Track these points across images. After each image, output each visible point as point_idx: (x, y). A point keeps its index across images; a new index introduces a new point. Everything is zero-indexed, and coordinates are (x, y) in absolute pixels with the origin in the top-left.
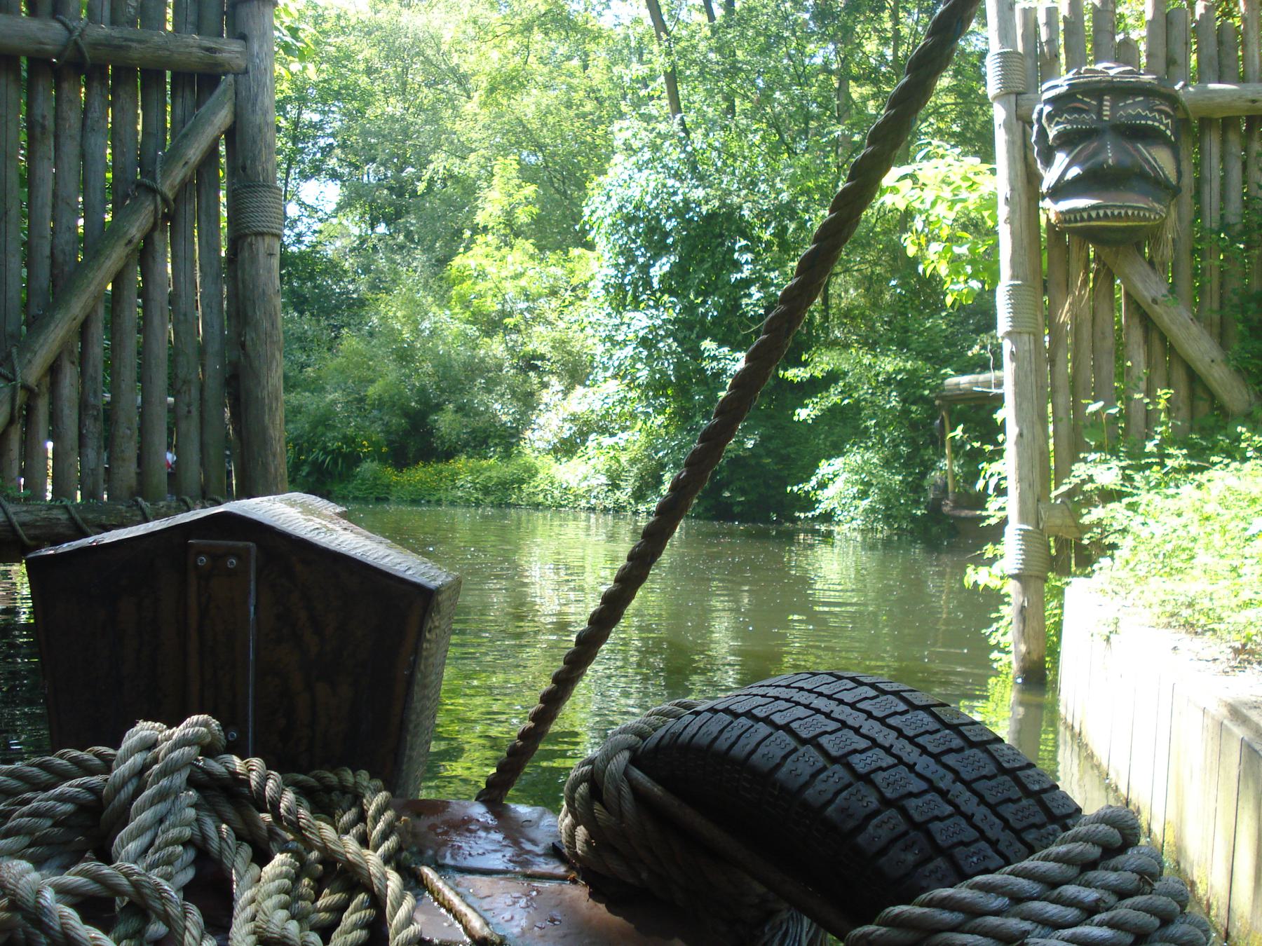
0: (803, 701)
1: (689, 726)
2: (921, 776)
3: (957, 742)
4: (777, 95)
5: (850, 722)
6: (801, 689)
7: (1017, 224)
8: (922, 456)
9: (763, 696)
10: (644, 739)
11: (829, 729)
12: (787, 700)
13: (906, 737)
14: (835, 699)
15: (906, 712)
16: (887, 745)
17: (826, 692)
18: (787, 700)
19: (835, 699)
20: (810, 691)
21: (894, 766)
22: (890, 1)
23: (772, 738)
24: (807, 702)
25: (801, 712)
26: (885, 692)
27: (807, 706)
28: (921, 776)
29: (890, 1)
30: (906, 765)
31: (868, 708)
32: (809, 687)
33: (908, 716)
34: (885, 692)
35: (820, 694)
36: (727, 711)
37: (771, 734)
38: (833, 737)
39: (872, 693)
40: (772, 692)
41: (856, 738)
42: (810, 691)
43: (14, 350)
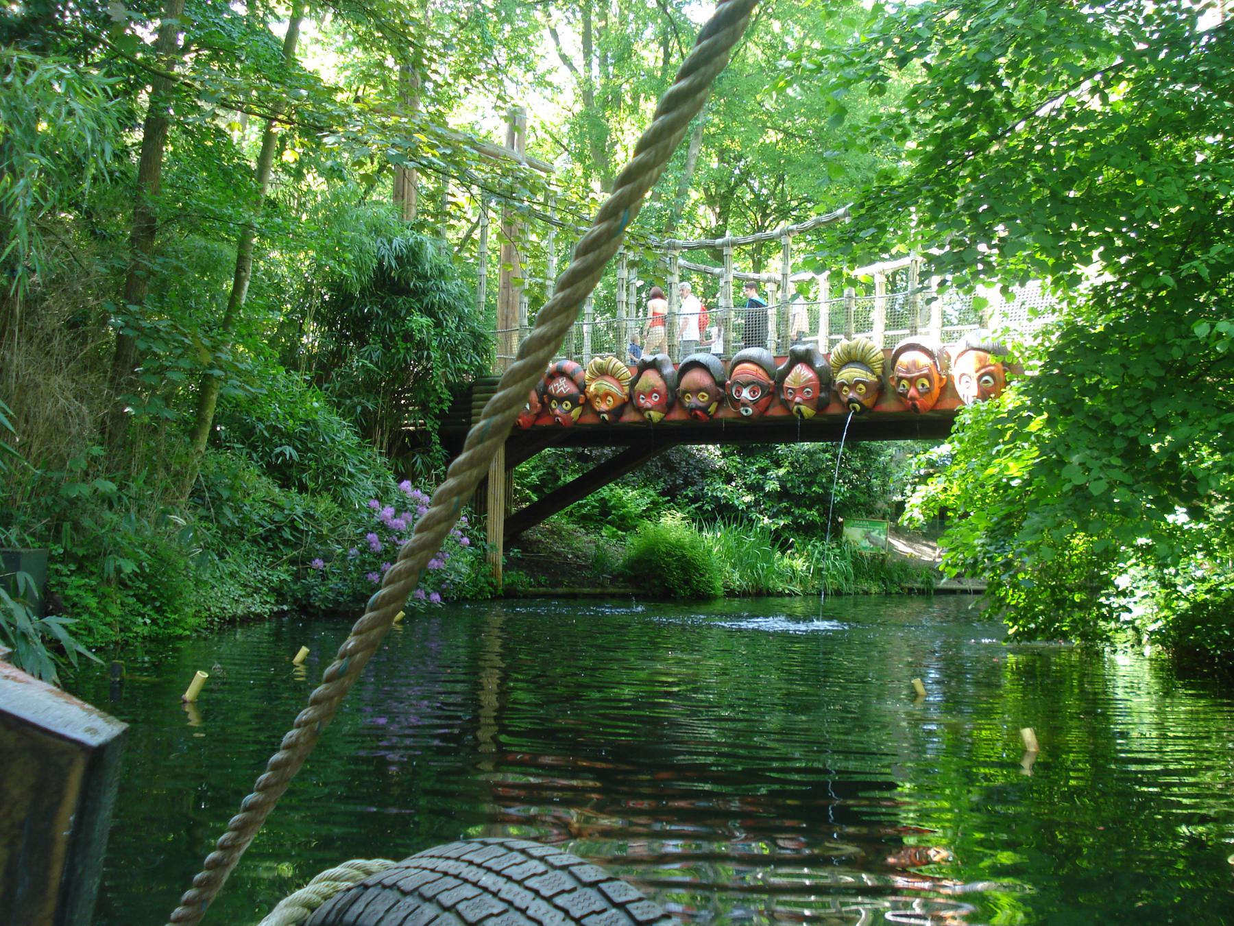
0: (471, 877)
2: (502, 900)
3: (569, 884)
5: (518, 902)
6: (471, 863)
7: (930, 414)
10: (312, 909)
11: (495, 911)
12: (456, 877)
13: (543, 898)
14: (504, 876)
16: (524, 907)
18: (456, 877)
20: (479, 866)
21: (505, 911)
23: (438, 921)
25: (468, 891)
27: (475, 884)
28: (502, 900)
30: (518, 909)
31: (567, 905)
33: (575, 894)
34: (554, 867)
35: (489, 870)
36: (393, 886)
37: (437, 917)
38: (498, 920)
39: (541, 868)
40: (442, 865)
41: (495, 901)
43: (1033, 200)
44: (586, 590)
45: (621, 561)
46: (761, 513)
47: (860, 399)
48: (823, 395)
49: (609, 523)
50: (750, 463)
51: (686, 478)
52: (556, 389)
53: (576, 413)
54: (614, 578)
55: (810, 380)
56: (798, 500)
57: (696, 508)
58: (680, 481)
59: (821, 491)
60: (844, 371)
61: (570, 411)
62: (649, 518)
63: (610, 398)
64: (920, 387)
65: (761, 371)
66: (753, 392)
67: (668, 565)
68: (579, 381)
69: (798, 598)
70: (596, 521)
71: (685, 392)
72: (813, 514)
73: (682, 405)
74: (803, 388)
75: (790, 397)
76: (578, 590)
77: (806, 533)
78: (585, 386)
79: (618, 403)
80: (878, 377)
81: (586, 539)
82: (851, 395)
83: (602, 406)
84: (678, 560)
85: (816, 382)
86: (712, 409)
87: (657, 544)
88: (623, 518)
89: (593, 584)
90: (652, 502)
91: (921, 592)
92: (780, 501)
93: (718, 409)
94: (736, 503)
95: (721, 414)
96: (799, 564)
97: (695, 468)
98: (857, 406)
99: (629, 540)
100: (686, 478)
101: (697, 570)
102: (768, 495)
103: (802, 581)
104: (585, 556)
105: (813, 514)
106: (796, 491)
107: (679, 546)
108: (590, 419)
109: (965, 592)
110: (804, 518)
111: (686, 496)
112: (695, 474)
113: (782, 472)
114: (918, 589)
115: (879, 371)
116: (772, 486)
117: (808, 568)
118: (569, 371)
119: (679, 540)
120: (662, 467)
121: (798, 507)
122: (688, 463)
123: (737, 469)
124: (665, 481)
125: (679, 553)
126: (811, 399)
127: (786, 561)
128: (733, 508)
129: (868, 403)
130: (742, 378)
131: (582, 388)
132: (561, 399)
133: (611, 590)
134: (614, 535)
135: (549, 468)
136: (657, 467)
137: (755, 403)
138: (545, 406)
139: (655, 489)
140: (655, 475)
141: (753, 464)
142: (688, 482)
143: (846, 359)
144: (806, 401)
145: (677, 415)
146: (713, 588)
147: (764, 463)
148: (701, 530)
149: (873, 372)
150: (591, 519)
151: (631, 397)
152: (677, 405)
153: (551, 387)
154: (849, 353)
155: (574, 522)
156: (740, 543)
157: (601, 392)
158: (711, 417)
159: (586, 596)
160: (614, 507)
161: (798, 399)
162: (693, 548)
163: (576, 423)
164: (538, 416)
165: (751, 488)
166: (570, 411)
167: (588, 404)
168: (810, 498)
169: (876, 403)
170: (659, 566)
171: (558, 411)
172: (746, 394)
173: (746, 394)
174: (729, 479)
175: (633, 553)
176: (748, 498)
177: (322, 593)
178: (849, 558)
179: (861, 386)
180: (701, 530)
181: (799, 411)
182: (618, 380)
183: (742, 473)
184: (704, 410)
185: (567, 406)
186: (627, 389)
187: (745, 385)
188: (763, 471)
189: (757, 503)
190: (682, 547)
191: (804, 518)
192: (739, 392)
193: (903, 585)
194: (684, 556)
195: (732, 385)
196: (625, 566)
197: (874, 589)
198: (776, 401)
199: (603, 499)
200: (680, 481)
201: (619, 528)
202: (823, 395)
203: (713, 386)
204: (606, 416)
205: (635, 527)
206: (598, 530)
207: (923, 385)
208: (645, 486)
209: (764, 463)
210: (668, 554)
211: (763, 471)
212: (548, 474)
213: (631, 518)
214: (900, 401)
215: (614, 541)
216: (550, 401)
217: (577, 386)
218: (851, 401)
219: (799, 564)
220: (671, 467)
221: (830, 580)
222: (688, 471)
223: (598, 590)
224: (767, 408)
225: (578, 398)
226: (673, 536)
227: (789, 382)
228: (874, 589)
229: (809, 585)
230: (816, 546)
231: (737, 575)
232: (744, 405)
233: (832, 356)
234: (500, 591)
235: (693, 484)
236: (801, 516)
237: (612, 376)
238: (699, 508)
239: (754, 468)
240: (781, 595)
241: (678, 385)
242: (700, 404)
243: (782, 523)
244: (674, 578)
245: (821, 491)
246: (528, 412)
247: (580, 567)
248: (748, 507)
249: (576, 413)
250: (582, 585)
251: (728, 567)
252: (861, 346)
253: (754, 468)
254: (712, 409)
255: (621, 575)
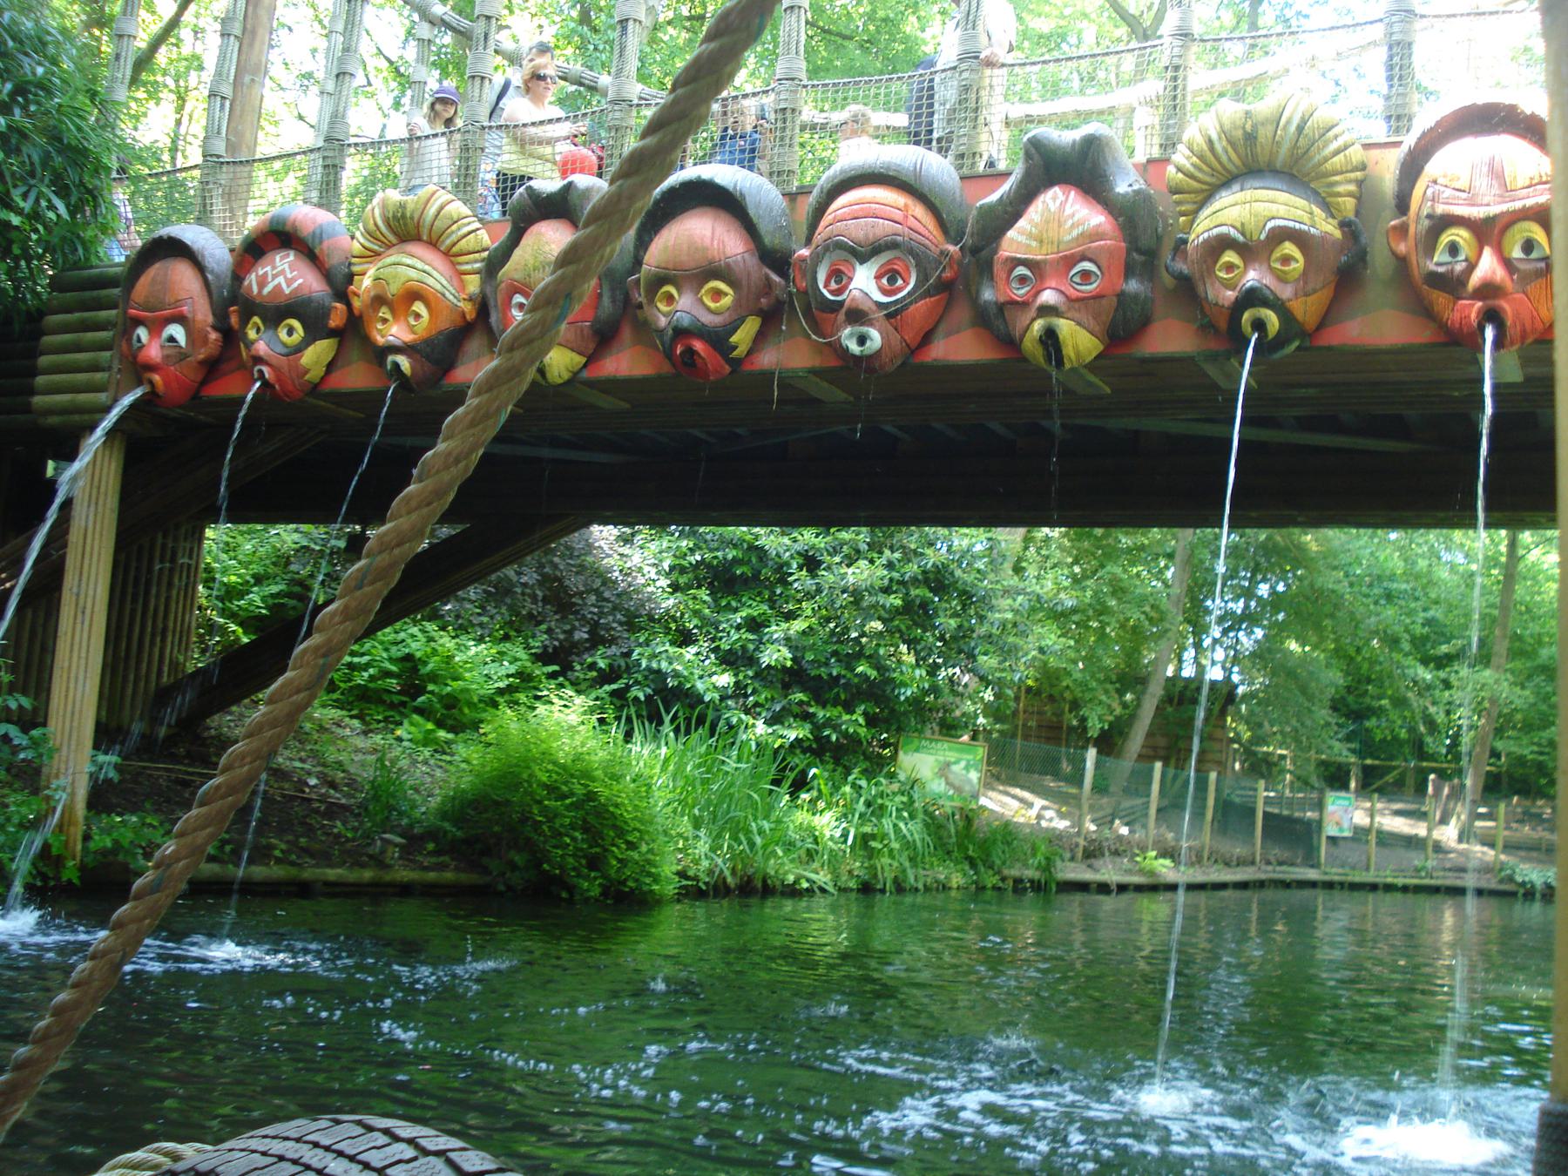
1: (247, 237)
4: (338, 1013)
6: (316, 1145)
8: (416, 1042)
9: (264, 1154)
14: (359, 1162)
15: (415, 1159)
17: (326, 1142)
19: (359, 1162)
20: (327, 1149)
22: (3, 992)
24: (296, 1156)
26: (426, 1152)
29: (3, 992)
32: (352, 1152)
34: (426, 1152)
35: (340, 1154)
39: (410, 1152)
42: (327, 1149)
44: (332, 874)
45: (434, 802)
46: (747, 712)
47: (1286, 292)
48: (1133, 286)
49: (420, 711)
50: (730, 609)
51: (594, 627)
52: (262, 283)
53: (317, 354)
54: (414, 841)
55: (1095, 235)
56: (820, 690)
57: (613, 694)
58: (581, 635)
59: (873, 674)
60: (1224, 199)
61: (299, 349)
62: (514, 704)
63: (419, 307)
64: (1517, 253)
65: (919, 210)
66: (890, 275)
67: (552, 816)
68: (334, 260)
69: (820, 900)
70: (392, 706)
71: (659, 281)
72: (854, 722)
73: (644, 329)
74: (1070, 261)
75: (1020, 293)
76: (312, 872)
77: (837, 761)
78: (350, 278)
79: (445, 323)
80: (1344, 225)
81: (360, 742)
82: (1253, 277)
83: (392, 331)
84: (576, 806)
85: (1113, 242)
86: (742, 337)
87: (526, 762)
88: (451, 702)
89: (355, 857)
90: (519, 674)
91: (1037, 887)
92: (786, 687)
93: (760, 338)
94: (700, 686)
95: (768, 359)
96: (827, 824)
97: (615, 608)
98: (1272, 319)
99: (462, 751)
100: (594, 627)
101: (621, 832)
102: (765, 675)
103: (834, 861)
104: (352, 783)
105: (854, 722)
106: (823, 671)
107: (578, 770)
108: (356, 377)
109: (1103, 888)
110: (836, 728)
111: (592, 666)
112: (613, 621)
113: (798, 625)
114: (1032, 881)
115: (1349, 204)
116: (774, 655)
117: (845, 835)
118: (306, 231)
119: (578, 758)
120: (545, 600)
121: (823, 704)
122: (601, 598)
123: (703, 618)
124: (549, 631)
125: (579, 790)
126: (1098, 297)
127: (801, 817)
128: (694, 699)
129: (1306, 310)
130: (859, 231)
131: (340, 285)
132: (276, 313)
133: (405, 874)
134: (428, 740)
135: (293, 582)
136: (534, 598)
137: (893, 314)
138: (231, 337)
139: (528, 647)
140: (531, 616)
141: (736, 610)
142: (596, 641)
143: (1231, 159)
144: (1076, 303)
145: (625, 363)
146: (656, 879)
147: (758, 609)
148: (628, 736)
149: (1327, 207)
150: (382, 702)
151: (483, 306)
152: (627, 333)
153: (252, 280)
154: (1250, 138)
155: (339, 705)
156: (711, 766)
157: (394, 289)
158: (736, 363)
159: (337, 890)
160: (433, 677)
161: (1048, 297)
162: (616, 778)
163: (315, 389)
164: (211, 368)
165: (729, 660)
166: (299, 349)
167: (353, 332)
168: (847, 686)
169: (1324, 321)
170: (525, 819)
171: (262, 348)
172: (864, 282)
173: (864, 282)
174: (685, 638)
175: (466, 783)
176: (725, 679)
177: (1539, 679)
178: (921, 816)
179: (1289, 248)
180: (628, 736)
181: (1050, 336)
182: (449, 255)
183: (711, 627)
184: (719, 339)
185: (292, 332)
186: (473, 284)
187: (862, 254)
188: (755, 625)
189: (739, 691)
190: (587, 775)
191: (836, 728)
192: (839, 276)
193: (1006, 872)
194: (591, 796)
195: (817, 259)
196: (443, 814)
197: (957, 880)
198: (961, 313)
199: (409, 658)
200: (581, 635)
201: (440, 724)
202: (1133, 286)
203: (752, 261)
204: (404, 363)
205: (475, 725)
206: (391, 723)
207: (1529, 246)
208: (506, 638)
209: (758, 609)
210: (551, 789)
211: (755, 625)
212: (289, 595)
213: (471, 705)
214: (1426, 312)
215: (427, 752)
216: (245, 320)
217: (326, 274)
218: (1252, 298)
219: (827, 824)
220: (560, 600)
221: (886, 860)
222: (601, 614)
223: (367, 875)
224: (927, 338)
225: (325, 313)
226: (564, 749)
227: (1018, 240)
228: (957, 880)
229: (844, 869)
230: (857, 786)
231: (703, 847)
232: (857, 316)
233: (1181, 156)
234: (70, 873)
235: (612, 641)
236: (829, 723)
237: (433, 244)
238: (618, 695)
239: (738, 618)
240: (793, 892)
241: (638, 263)
242: (707, 319)
243: (792, 735)
244: (564, 854)
245: (873, 674)
246: (182, 356)
247: (334, 811)
248: (722, 699)
249: (317, 354)
250: (325, 858)
251: (685, 825)
252: (1293, 115)
253: (738, 618)
254: (742, 337)
255: (432, 834)
